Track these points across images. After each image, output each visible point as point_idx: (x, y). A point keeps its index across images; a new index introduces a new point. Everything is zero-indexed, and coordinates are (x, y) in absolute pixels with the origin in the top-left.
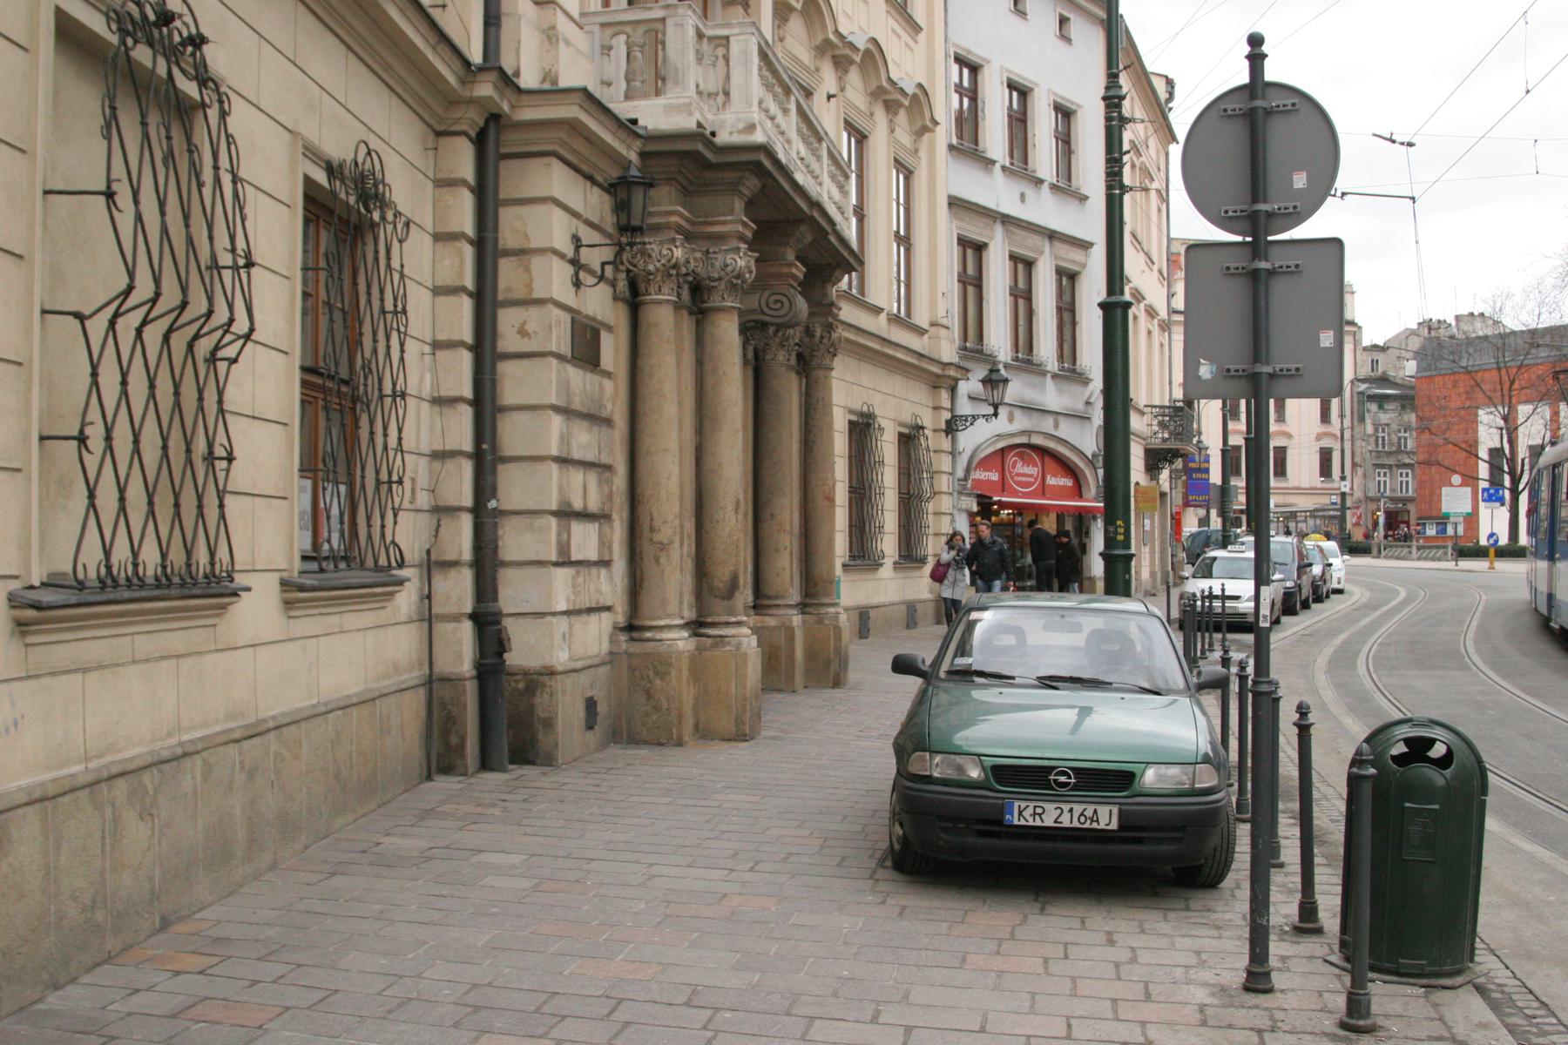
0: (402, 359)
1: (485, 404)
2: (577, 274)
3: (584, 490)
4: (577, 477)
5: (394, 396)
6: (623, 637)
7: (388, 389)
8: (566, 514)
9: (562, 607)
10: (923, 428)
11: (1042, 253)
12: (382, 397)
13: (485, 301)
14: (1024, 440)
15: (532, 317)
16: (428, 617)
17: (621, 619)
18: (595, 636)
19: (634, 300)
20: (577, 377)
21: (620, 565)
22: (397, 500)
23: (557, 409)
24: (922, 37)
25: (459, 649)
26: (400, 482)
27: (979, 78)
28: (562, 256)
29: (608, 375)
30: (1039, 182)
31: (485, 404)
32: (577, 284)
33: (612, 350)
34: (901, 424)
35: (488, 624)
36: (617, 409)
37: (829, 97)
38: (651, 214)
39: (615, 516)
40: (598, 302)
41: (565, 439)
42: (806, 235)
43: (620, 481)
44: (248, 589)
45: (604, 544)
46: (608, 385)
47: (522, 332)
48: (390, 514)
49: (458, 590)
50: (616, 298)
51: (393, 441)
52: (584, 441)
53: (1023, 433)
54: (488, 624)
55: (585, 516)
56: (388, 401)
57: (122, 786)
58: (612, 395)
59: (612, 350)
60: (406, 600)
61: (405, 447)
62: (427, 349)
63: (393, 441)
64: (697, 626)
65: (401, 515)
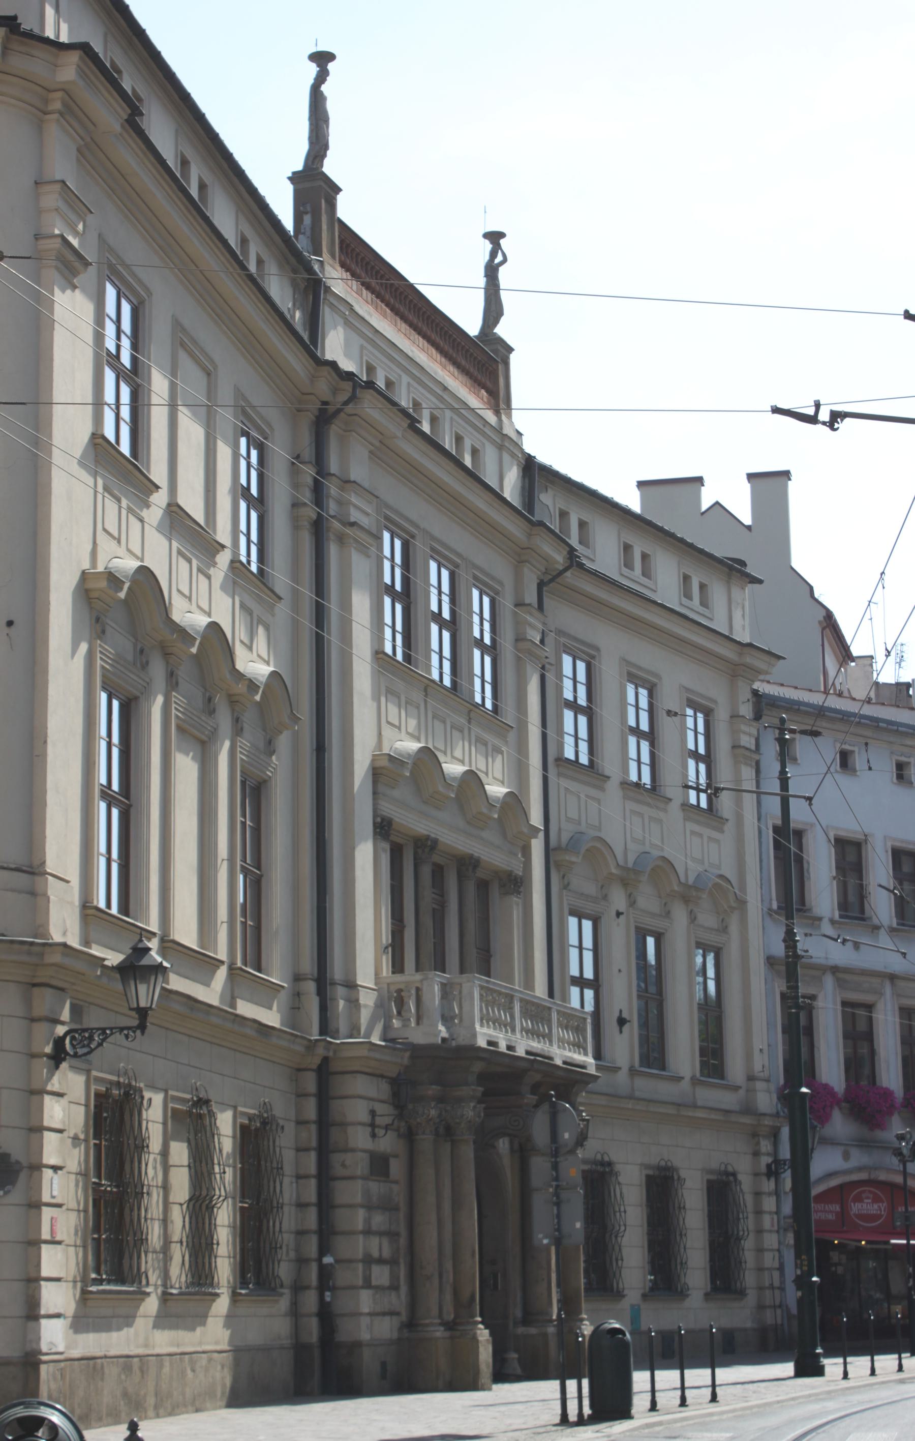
0: (281, 1191)
1: (325, 1204)
2: (373, 1130)
3: (377, 1246)
4: (375, 1242)
5: (278, 1207)
6: (405, 1331)
7: (275, 1205)
8: (368, 1261)
9: (366, 1310)
10: (734, 1174)
11: (881, 994)
12: (272, 1208)
13: (324, 1150)
14: (863, 1176)
15: (348, 1158)
16: (295, 1312)
17: (404, 1318)
18: (386, 1328)
19: (410, 1137)
20: (375, 1187)
21: (404, 1289)
22: (279, 1256)
23: (362, 1206)
24: (729, 827)
25: (312, 1331)
26: (281, 1247)
27: (804, 841)
28: (363, 1124)
29: (396, 1182)
30: (876, 928)
31: (325, 1204)
32: (374, 1135)
33: (397, 1168)
34: (711, 1172)
35: (326, 1315)
36: (400, 1198)
37: (619, 914)
38: (698, 783)
39: (402, 1261)
40: (387, 1143)
41: (368, 1221)
42: (46, 1422)
43: (403, 1241)
44: (621, 1011)
45: (394, 1277)
46: (395, 1187)
47: (343, 1165)
48: (276, 1263)
49: (310, 1301)
50: (399, 1136)
51: (277, 1228)
52: (379, 1220)
53: (860, 1169)
54: (326, 1315)
55: (381, 1261)
56: (275, 1210)
57: (187, 1356)
58: (399, 1193)
59: (397, 1168)
60: (284, 1303)
61: (283, 1230)
62: (294, 1180)
63: (277, 1228)
64: (450, 1326)
65: (282, 1263)
